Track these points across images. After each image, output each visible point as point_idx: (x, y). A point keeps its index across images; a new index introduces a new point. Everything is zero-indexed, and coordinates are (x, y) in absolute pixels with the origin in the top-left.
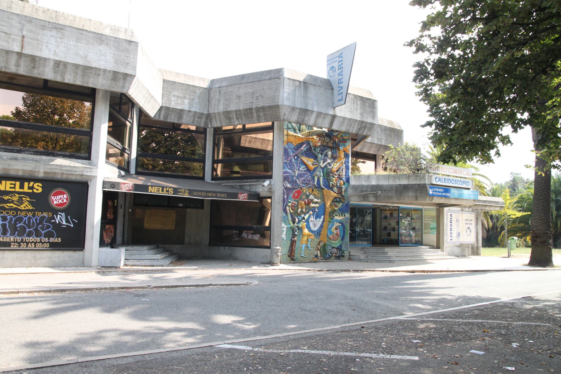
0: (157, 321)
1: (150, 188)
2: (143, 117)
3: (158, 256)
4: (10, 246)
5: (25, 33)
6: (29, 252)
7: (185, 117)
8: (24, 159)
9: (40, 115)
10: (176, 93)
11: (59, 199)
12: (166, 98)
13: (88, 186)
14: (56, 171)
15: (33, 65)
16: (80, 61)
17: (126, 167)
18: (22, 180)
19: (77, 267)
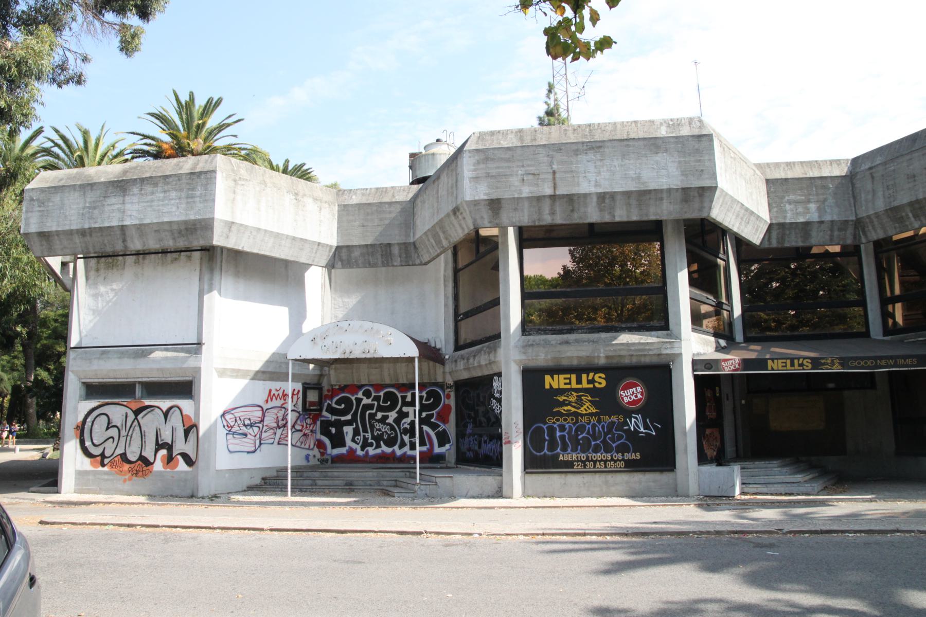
0: (790, 591)
1: (770, 362)
2: (744, 247)
3: (799, 477)
4: (572, 467)
5: (555, 167)
6: (598, 475)
7: (814, 233)
8: (577, 341)
9: (594, 271)
10: (792, 197)
11: (632, 394)
12: (775, 209)
13: (670, 371)
14: (622, 353)
15: (571, 208)
16: (632, 187)
17: (727, 333)
18: (578, 371)
19: (667, 496)
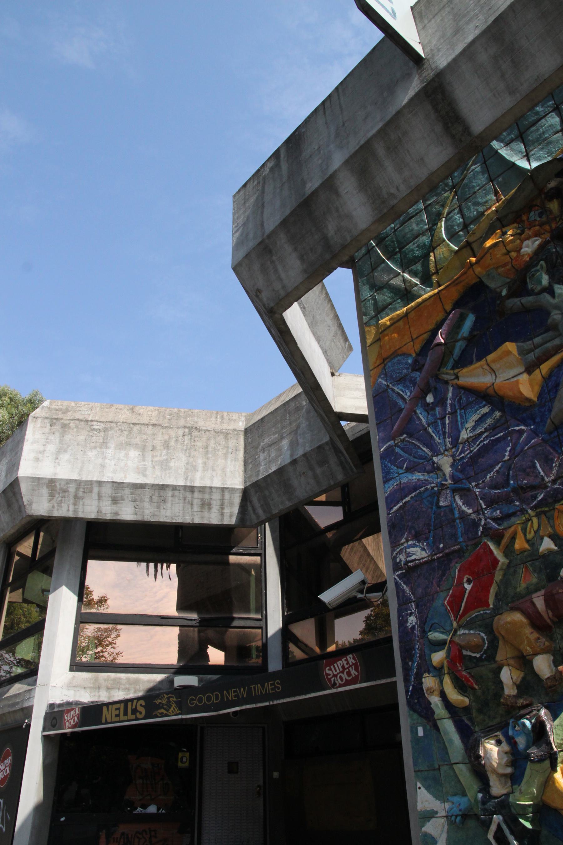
7: (295, 482)
